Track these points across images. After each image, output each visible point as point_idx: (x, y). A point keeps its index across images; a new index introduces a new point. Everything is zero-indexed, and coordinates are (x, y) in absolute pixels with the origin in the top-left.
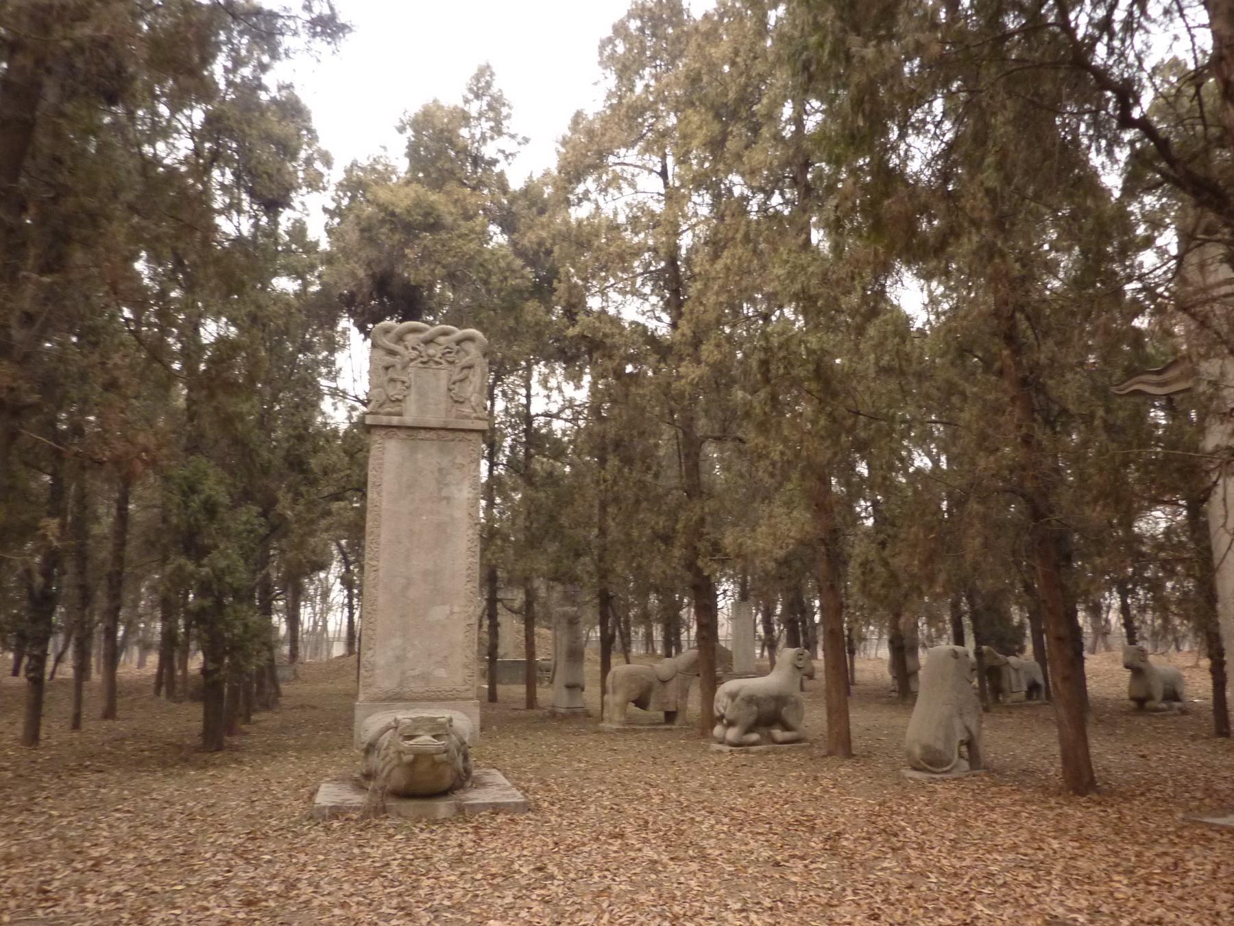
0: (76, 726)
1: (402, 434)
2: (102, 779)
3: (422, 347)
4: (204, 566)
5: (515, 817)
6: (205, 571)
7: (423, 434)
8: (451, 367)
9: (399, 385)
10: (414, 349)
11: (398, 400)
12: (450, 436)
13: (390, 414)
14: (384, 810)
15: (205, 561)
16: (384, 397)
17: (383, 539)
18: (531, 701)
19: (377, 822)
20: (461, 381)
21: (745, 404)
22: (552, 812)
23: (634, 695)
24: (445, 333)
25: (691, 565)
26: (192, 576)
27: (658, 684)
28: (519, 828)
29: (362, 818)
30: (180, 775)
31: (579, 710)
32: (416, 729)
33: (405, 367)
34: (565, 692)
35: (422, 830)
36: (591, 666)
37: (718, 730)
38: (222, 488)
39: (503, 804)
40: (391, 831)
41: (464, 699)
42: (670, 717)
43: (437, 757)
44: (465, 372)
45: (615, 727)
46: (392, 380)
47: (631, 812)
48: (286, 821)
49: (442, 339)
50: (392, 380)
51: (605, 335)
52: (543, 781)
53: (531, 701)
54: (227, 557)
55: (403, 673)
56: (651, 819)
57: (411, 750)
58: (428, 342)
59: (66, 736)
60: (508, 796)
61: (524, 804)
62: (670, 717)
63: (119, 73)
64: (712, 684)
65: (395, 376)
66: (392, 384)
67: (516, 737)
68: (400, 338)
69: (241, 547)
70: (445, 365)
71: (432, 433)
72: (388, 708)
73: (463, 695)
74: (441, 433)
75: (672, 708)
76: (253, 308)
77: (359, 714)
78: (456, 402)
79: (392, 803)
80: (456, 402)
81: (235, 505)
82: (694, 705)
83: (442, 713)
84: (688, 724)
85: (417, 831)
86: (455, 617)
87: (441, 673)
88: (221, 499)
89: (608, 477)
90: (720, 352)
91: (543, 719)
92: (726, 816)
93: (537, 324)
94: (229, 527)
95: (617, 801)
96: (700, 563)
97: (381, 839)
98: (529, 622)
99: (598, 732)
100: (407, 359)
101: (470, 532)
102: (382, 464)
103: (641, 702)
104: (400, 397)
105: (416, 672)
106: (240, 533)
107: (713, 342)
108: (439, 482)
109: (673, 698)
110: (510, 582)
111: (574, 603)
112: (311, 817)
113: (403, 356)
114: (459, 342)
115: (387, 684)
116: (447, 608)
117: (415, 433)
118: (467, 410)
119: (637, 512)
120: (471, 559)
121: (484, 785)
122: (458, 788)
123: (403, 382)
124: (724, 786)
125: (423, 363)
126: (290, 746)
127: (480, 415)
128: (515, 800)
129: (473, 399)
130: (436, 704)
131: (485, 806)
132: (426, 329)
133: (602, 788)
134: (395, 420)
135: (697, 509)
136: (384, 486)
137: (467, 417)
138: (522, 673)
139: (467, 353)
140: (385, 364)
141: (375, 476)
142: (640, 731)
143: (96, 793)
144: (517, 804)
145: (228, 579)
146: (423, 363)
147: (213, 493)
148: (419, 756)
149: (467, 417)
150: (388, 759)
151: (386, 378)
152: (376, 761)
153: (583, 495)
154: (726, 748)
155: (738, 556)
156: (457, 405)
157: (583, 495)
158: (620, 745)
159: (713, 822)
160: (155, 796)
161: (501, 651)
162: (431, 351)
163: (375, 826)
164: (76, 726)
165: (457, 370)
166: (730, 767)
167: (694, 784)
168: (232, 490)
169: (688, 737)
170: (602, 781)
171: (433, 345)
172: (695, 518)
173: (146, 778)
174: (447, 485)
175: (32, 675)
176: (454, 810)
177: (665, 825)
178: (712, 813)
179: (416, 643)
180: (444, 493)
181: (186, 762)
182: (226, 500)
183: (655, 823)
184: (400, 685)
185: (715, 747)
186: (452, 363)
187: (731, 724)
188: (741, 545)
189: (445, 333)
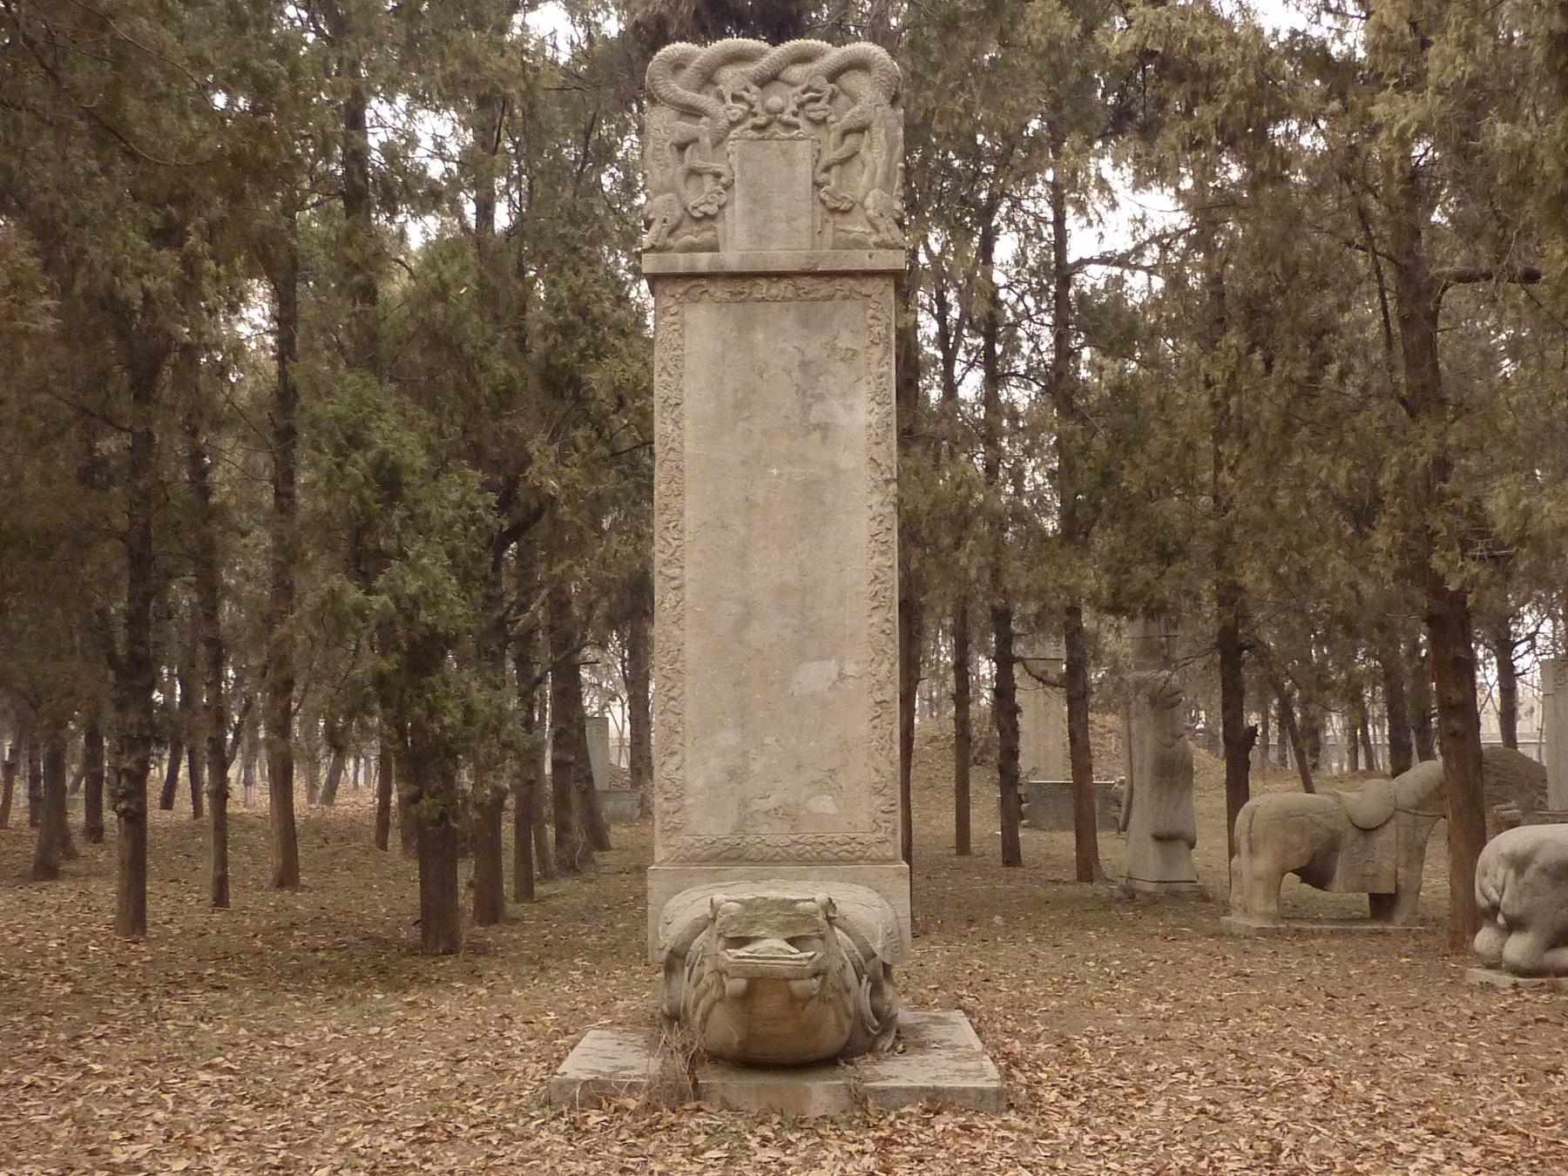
0: (220, 900)
1: (720, 291)
2: (213, 1004)
3: (754, 94)
4: (377, 592)
5: (977, 1121)
6: (380, 601)
7: (763, 288)
8: (820, 133)
9: (708, 181)
10: (736, 98)
11: (706, 216)
12: (824, 288)
13: (691, 248)
14: (698, 1092)
15: (380, 582)
16: (678, 212)
17: (691, 519)
18: (1087, 866)
19: (673, 1118)
20: (843, 162)
21: (1515, 155)
22: (1064, 1112)
23: (1298, 859)
24: (804, 58)
25: (1418, 572)
26: (360, 612)
27: (1351, 835)
28: (981, 1148)
29: (649, 1107)
30: (354, 1002)
31: (1185, 888)
32: (752, 923)
33: (718, 143)
34: (1152, 848)
35: (765, 1142)
36: (1208, 797)
37: (1484, 939)
38: (411, 438)
39: (951, 1091)
40: (700, 1140)
41: (875, 861)
42: (1383, 905)
43: (796, 986)
44: (851, 140)
45: (1257, 923)
46: (694, 173)
47: (1246, 1121)
48: (501, 1106)
49: (796, 72)
50: (694, 173)
51: (1195, 46)
52: (1064, 1042)
53: (1087, 866)
54: (422, 572)
55: (744, 803)
56: (1288, 1143)
57: (740, 970)
58: (767, 81)
59: (200, 919)
60: (965, 1074)
61: (999, 1093)
62: (1383, 905)
63: (1255, 311)
64: (1472, 838)
65: (699, 163)
66: (693, 183)
67: (1038, 941)
68: (707, 79)
69: (452, 554)
70: (805, 127)
71: (783, 284)
72: (714, 878)
73: (874, 851)
74: (805, 283)
75: (1385, 887)
76: (456, 65)
77: (655, 886)
78: (834, 211)
79: (711, 1078)
80: (834, 211)
81: (440, 468)
82: (1435, 879)
83: (808, 891)
84: (1423, 921)
85: (754, 1143)
86: (850, 684)
87: (825, 804)
88: (408, 459)
89: (1217, 374)
90: (1474, 59)
91: (1106, 905)
92: (1475, 1142)
93: (1053, 45)
94: (427, 515)
95: (1220, 1093)
96: (1436, 563)
97: (677, 1157)
98: (1078, 700)
99: (1218, 935)
100: (723, 122)
101: (876, 498)
102: (679, 358)
103: (1315, 873)
104: (712, 210)
105: (772, 803)
106: (450, 526)
107: (1452, 35)
108: (801, 392)
109: (1387, 865)
110: (1040, 622)
111: (1167, 662)
112: (549, 1102)
113: (714, 118)
114: (834, 76)
115: (711, 827)
116: (831, 667)
117: (746, 286)
118: (858, 228)
119: (1288, 452)
120: (878, 559)
121: (922, 1046)
122: (862, 1051)
123: (718, 175)
124: (1486, 1069)
125: (755, 128)
126: (585, 947)
127: (887, 237)
128: (980, 1084)
129: (869, 202)
130: (816, 871)
131: (911, 1093)
132: (762, 53)
133: (1192, 1062)
134: (703, 261)
135: (1427, 441)
136: (687, 405)
137: (859, 244)
138: (1067, 809)
139: (854, 99)
140: (676, 137)
141: (667, 386)
142: (1313, 934)
143: (191, 1030)
144: (982, 1093)
145: (425, 616)
146: (755, 128)
147: (391, 446)
148: (758, 984)
149: (859, 244)
150: (702, 985)
151: (680, 170)
152: (684, 989)
153: (1168, 424)
154: (1506, 980)
155: (1521, 541)
156: (838, 217)
157: (1168, 424)
158: (1261, 965)
159: (1439, 1156)
160: (288, 1041)
161: (1024, 763)
162: (775, 101)
163: (670, 1128)
164: (220, 900)
165: (834, 137)
166: (1506, 1025)
167: (1414, 1061)
168: (434, 440)
169: (1421, 951)
170: (1195, 1046)
171: (776, 86)
172: (1422, 460)
173: (292, 1004)
174: (821, 398)
175: (123, 806)
176: (845, 1101)
177: (1320, 1159)
178: (1440, 1133)
179: (769, 740)
180: (814, 417)
181: (385, 976)
182: (421, 461)
183: (1295, 1152)
184: (740, 828)
185: (1480, 975)
186: (821, 123)
187: (1515, 925)
188: (1527, 513)
189: (804, 58)
